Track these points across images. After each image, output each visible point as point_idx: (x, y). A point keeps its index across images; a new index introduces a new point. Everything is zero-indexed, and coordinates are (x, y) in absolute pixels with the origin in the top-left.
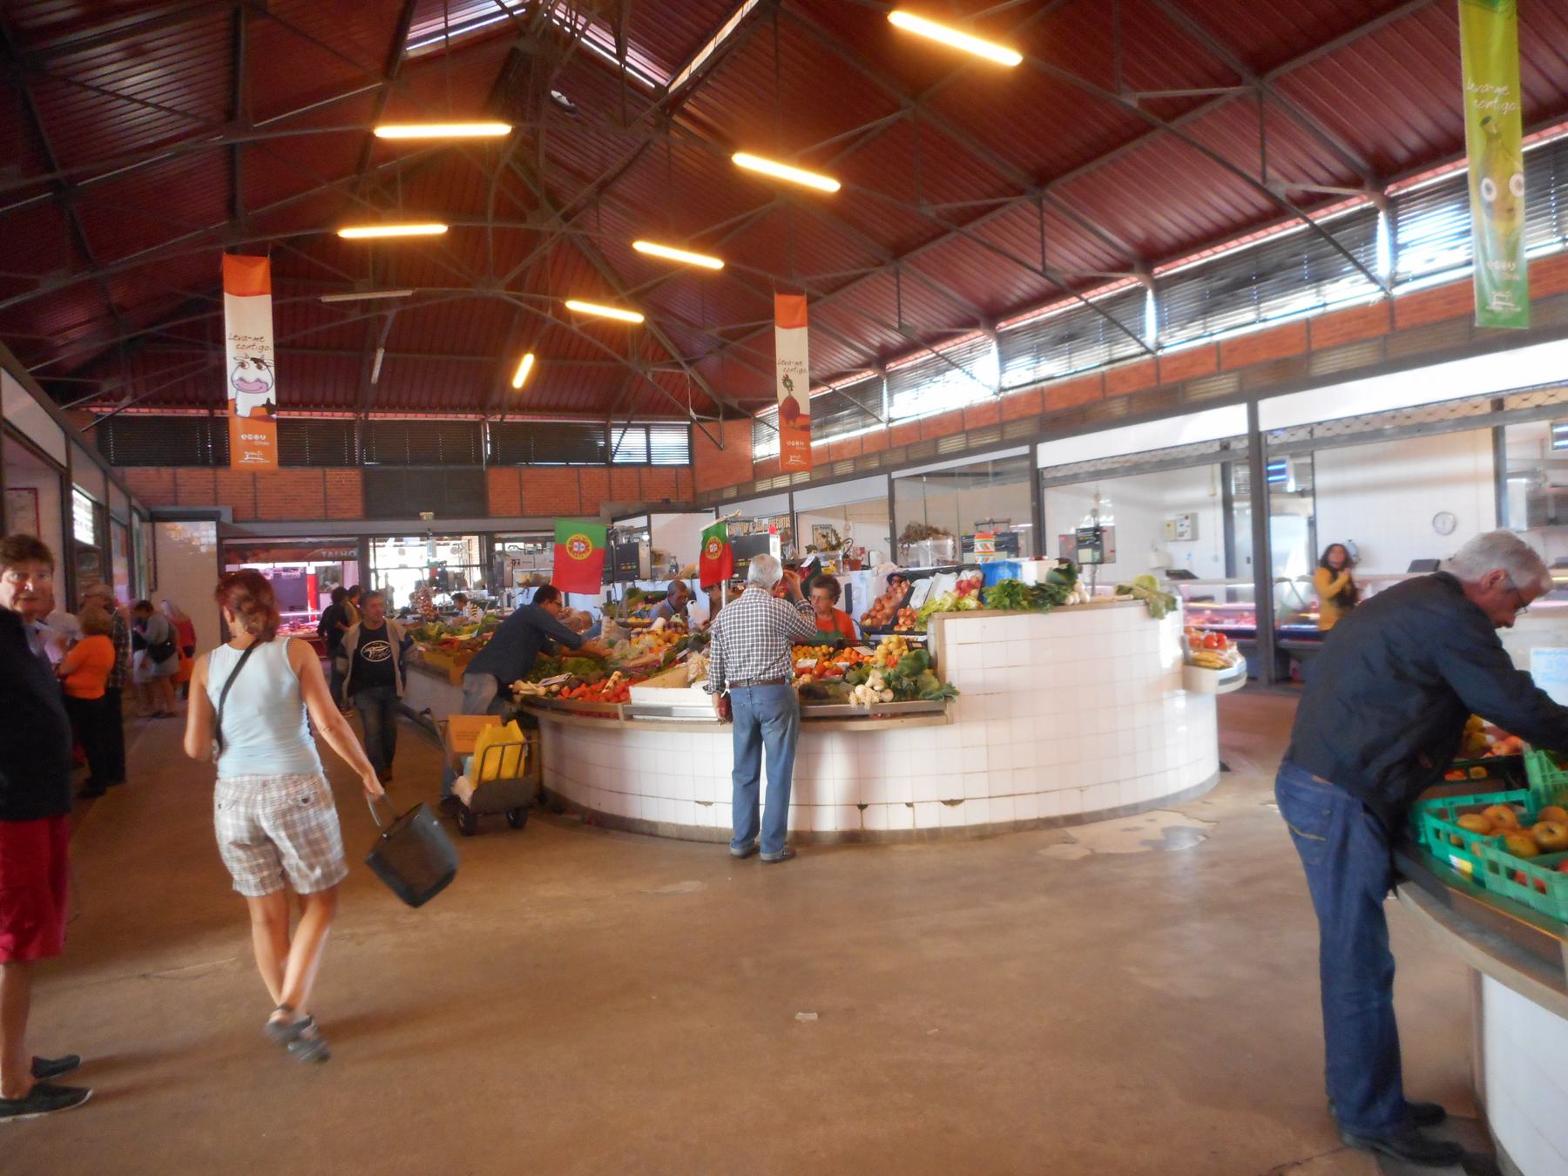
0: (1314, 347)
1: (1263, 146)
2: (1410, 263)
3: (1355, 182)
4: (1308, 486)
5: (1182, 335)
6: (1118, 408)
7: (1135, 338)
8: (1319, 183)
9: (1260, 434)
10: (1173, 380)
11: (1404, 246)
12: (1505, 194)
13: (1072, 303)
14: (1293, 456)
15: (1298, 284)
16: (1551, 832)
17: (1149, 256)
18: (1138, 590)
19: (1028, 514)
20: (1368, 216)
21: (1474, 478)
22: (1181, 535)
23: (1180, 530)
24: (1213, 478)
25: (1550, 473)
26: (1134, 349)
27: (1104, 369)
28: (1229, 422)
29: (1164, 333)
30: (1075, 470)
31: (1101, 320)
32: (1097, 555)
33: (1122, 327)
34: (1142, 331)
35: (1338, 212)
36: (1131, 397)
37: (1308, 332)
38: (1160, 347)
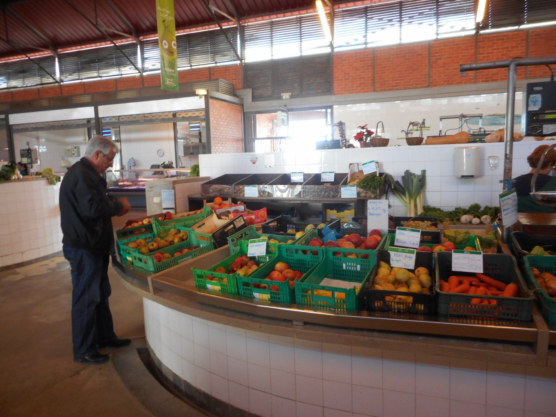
0: (118, 89)
1: (96, 10)
2: (148, 65)
3: (130, 33)
4: (118, 138)
5: (70, 77)
6: (45, 103)
7: (51, 76)
8: (118, 30)
9: (99, 118)
10: (66, 94)
11: (146, 59)
12: (170, 47)
13: (23, 58)
14: (113, 128)
15: (112, 66)
16: (153, 245)
17: (55, 44)
18: (44, 174)
19: (6, 144)
20: (134, 46)
21: (168, 139)
22: (74, 154)
23: (73, 152)
24: (85, 133)
25: (191, 139)
26: (51, 80)
27: (39, 87)
28: (87, 112)
29: (61, 75)
30: (26, 126)
31: (36, 66)
32: (30, 160)
33: (46, 71)
34: (55, 74)
35: (124, 42)
36: (49, 99)
37: (116, 83)
38: (62, 81)
